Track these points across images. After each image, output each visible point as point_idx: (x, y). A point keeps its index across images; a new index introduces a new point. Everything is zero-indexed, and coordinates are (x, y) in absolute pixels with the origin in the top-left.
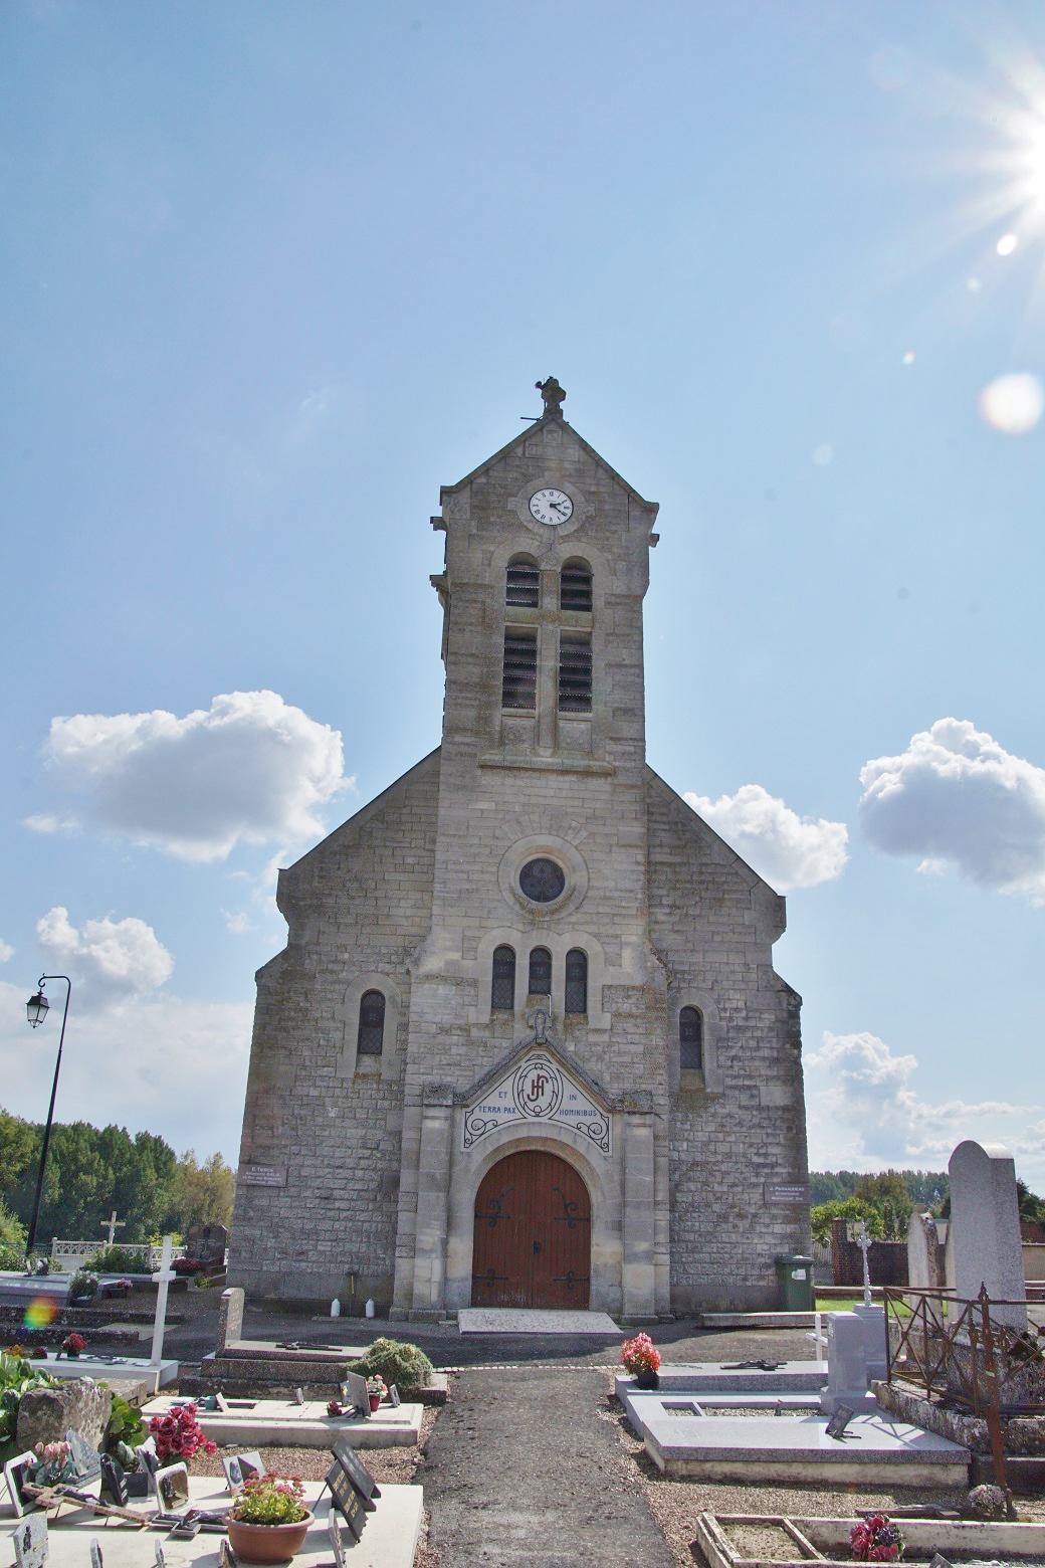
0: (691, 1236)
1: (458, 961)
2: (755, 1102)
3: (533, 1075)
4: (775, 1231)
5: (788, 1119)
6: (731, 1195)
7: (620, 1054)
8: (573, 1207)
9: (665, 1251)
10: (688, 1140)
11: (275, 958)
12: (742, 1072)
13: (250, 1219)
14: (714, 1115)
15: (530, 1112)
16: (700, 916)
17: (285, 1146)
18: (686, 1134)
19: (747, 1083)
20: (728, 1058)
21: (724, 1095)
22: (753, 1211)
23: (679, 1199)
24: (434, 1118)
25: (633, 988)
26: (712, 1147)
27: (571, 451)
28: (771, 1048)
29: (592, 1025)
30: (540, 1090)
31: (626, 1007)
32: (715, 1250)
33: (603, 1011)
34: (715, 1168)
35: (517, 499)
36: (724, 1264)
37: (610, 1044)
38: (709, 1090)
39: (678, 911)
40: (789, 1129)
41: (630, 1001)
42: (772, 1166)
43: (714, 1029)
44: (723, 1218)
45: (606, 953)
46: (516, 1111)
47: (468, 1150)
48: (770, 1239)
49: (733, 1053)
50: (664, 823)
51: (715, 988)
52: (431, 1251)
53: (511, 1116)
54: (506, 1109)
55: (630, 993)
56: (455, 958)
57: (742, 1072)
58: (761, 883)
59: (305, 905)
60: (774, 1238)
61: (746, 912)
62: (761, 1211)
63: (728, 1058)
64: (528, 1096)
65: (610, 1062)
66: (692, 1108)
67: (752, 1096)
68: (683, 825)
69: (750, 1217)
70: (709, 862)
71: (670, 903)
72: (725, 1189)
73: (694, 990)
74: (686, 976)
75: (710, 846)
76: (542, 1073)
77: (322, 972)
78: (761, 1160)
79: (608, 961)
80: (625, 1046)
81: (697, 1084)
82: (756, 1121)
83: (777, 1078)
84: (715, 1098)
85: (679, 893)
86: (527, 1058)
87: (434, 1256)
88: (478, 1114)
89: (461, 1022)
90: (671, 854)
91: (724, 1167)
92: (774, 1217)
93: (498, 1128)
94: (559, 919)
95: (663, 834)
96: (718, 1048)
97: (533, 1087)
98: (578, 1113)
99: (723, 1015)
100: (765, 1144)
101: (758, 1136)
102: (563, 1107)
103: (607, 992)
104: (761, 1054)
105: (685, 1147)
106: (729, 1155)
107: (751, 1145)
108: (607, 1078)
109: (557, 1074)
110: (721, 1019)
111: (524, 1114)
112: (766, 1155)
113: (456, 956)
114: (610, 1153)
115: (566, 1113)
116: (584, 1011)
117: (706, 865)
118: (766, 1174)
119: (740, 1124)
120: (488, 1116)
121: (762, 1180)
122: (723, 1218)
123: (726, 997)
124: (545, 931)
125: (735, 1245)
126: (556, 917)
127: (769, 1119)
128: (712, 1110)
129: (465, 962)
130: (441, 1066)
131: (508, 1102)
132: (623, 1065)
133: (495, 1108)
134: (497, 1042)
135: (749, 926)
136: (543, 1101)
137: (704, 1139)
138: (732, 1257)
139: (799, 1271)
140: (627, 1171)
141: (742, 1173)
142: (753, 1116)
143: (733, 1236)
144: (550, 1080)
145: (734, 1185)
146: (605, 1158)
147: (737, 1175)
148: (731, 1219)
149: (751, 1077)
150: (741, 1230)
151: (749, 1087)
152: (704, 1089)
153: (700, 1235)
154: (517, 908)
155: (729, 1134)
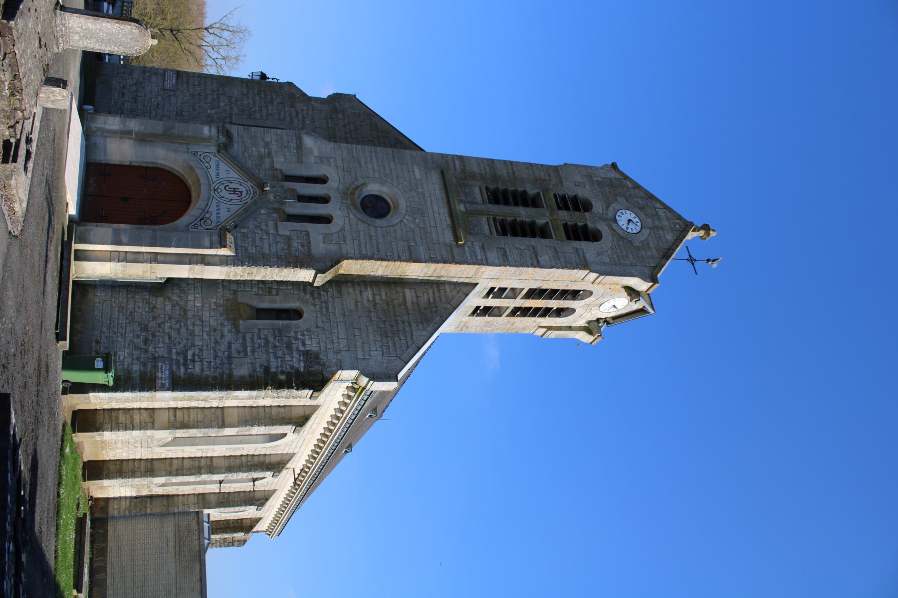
0: (131, 306)
2: (234, 354)
3: (242, 189)
4: (134, 366)
5: (223, 378)
6: (163, 335)
7: (262, 239)
10: (203, 306)
11: (301, 90)
12: (256, 345)
13: (145, 74)
14: (222, 325)
15: (218, 185)
16: (371, 321)
17: (188, 90)
19: (249, 349)
20: (266, 336)
21: (238, 332)
22: (150, 350)
23: (158, 299)
24: (210, 131)
25: (309, 249)
26: (198, 322)
27: (671, 234)
28: (277, 367)
29: (279, 224)
30: (233, 192)
31: (295, 244)
32: (120, 322)
34: (182, 324)
35: (626, 203)
36: (109, 328)
37: (268, 233)
38: (241, 322)
39: (372, 306)
40: (215, 378)
41: (300, 247)
42: (185, 365)
44: (145, 328)
45: (332, 234)
46: (217, 179)
48: (128, 361)
49: (271, 339)
50: (434, 299)
51: (319, 329)
52: (124, 125)
53: (214, 176)
56: (315, 152)
57: (256, 345)
58: (404, 364)
59: (336, 105)
60: (129, 365)
61: (380, 353)
62: (149, 354)
63: (266, 336)
64: (228, 186)
65: (255, 233)
67: (239, 352)
68: (436, 312)
69: (145, 347)
70: (413, 328)
71: (377, 301)
72: (167, 331)
73: (315, 315)
75: (424, 329)
76: (244, 194)
77: (296, 111)
78: (190, 357)
79: (326, 236)
82: (220, 354)
83: (254, 371)
84: (236, 326)
85: (385, 307)
86: (253, 186)
87: (121, 126)
88: (214, 159)
89: (273, 153)
90: (412, 303)
91: (183, 330)
92: (145, 365)
93: (206, 169)
94: (350, 208)
95: (426, 299)
97: (234, 189)
98: (218, 213)
99: (299, 333)
100: (202, 361)
101: (208, 355)
102: (221, 205)
104: (272, 359)
105: (197, 305)
106: (192, 334)
107: (201, 350)
108: (244, 231)
109: (245, 202)
111: (216, 183)
112: (193, 361)
113: (316, 153)
117: (410, 326)
118: (179, 361)
119: (216, 342)
120: (213, 164)
121: (174, 357)
122: (145, 328)
123: (313, 337)
124: (341, 201)
125: (124, 336)
126: (351, 207)
127: (222, 364)
128: (226, 323)
131: (223, 174)
132: (254, 241)
133: (219, 168)
135: (370, 355)
136: (225, 194)
137: (204, 318)
138: (115, 333)
139: (102, 363)
141: (179, 343)
142: (224, 352)
143: (131, 335)
145: (170, 337)
147: (178, 340)
148: (144, 334)
149: (253, 352)
150: (136, 340)
151: (246, 350)
152: (242, 319)
153: (132, 312)
154: (353, 186)
155: (209, 335)
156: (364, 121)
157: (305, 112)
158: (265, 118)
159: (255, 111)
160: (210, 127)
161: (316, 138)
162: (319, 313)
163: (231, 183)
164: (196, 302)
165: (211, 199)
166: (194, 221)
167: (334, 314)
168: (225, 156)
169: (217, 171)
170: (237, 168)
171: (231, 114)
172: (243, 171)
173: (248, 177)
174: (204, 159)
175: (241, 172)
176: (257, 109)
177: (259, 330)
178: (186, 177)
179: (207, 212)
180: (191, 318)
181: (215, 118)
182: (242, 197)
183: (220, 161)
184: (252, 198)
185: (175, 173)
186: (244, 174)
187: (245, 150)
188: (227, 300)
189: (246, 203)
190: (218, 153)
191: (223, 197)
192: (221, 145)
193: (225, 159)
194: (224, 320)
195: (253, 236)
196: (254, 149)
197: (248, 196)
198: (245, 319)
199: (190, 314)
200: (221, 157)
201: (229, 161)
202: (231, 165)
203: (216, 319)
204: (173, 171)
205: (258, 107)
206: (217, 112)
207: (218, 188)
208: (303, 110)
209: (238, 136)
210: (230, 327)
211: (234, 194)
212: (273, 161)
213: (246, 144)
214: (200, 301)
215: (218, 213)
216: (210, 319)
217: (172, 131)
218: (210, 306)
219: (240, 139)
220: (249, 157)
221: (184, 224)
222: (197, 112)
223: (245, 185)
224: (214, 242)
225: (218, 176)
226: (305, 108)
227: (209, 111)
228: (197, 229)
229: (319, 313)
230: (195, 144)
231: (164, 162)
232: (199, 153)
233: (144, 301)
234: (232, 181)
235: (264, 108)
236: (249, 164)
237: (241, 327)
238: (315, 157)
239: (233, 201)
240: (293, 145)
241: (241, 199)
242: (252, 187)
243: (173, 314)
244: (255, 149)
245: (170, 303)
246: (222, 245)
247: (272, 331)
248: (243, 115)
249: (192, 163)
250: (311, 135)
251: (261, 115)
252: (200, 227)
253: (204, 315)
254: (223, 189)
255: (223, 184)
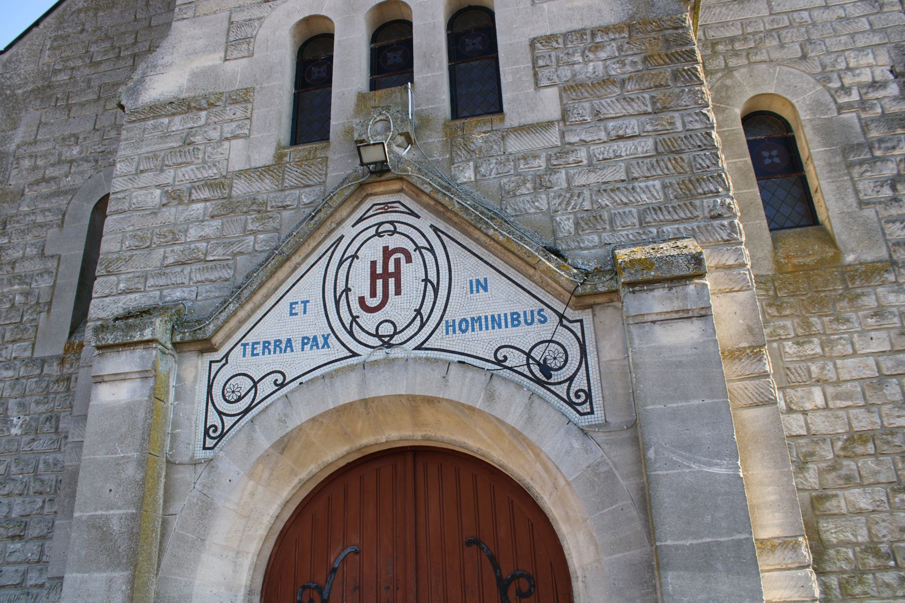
1: (215, 66)
3: (373, 251)
8: (524, 585)
9: (767, 574)
14: (879, 313)
18: (814, 368)
24: (119, 378)
25: (606, 30)
30: (392, 281)
31: (593, 68)
33: (537, 86)
37: (565, 149)
41: (603, 55)
43: (826, 131)
46: (332, 340)
47: (209, 454)
53: (319, 356)
54: (305, 341)
55: (598, 40)
64: (362, 300)
65: (569, 189)
66: (818, 303)
74: (738, 46)
80: (601, 148)
81: (815, 250)
88: (238, 361)
89: (212, 172)
96: (850, 166)
97: (374, 277)
98: (496, 322)
99: (843, 99)
103: (541, 49)
105: (819, 400)
108: (567, 224)
110: (840, 108)
113: (214, 59)
114: (599, 415)
115: (465, 325)
116: (501, 111)
128: (870, 302)
129: (230, 66)
130: (163, 270)
132: (603, 188)
134: (290, 198)
137: (868, 373)
140: (651, 454)
144: (416, 256)
146: (584, 432)
152: (838, 255)
156: (83, 24)
157: (40, 162)
158: (51, 264)
159: (27, 294)
160: (100, 380)
161: (155, 67)
162: (753, 59)
163: (347, 290)
164: (808, 406)
165: (431, 354)
166: (554, 407)
167: (744, 24)
168: (226, 322)
169: (297, 345)
170: (280, 274)
171: (31, 362)
172: (296, 251)
173: (319, 236)
174: (240, 399)
175: (296, 259)
176: (16, 287)
177: (862, 204)
178: (313, 468)
179: (499, 362)
180: (881, 417)
181: (42, 408)
182: (410, 247)
183: (250, 339)
184: (412, 213)
185: (287, 516)
186: (305, 250)
187: (200, 261)
188: (780, 307)
189: (436, 230)
190: (213, 349)
191: (418, 312)
192: (178, 338)
193: (242, 322)
194: (858, 309)
195: (587, 193)
196: (194, 233)
197: (401, 228)
198: (835, 246)
199: (863, 422)
200: (228, 337)
201: (248, 307)
202: (267, 297)
203: (862, 333)
204: (280, 525)
205: (12, 285)
206: (21, 405)
207: (377, 335)
208: (35, 168)
209: (137, 291)
210: (880, 290)
211: (397, 275)
212: (240, 174)
213: (170, 260)
214: (800, 392)
215: (496, 322)
216: (867, 355)
217: (115, 525)
218: (813, 358)
219: (151, 282)
220: (227, 245)
221: (577, 445)
222: (14, 469)
223: (357, 244)
224: (677, 305)
225: (321, 341)
226: (26, 163)
227: (14, 431)
228: (589, 396)
229: (753, 59)
230: (174, 437)
231: (247, 562)
232: (214, 419)
233: (858, 590)
234: (341, 287)
235: (16, 271)
236: (262, 241)
237: (869, 257)
238: (226, 60)
239: (432, 276)
240: (178, 124)
241: (418, 248)
242: (361, 220)
243: (882, 478)
244: (192, 231)
245: (839, 493)
246: (691, 272)
247: (856, 171)
248: (37, 326)
249: (264, 443)
250: (142, 80)
251: (41, 274)
252: (580, 383)
253: (855, 375)
254: (379, 316)
255: (354, 318)
